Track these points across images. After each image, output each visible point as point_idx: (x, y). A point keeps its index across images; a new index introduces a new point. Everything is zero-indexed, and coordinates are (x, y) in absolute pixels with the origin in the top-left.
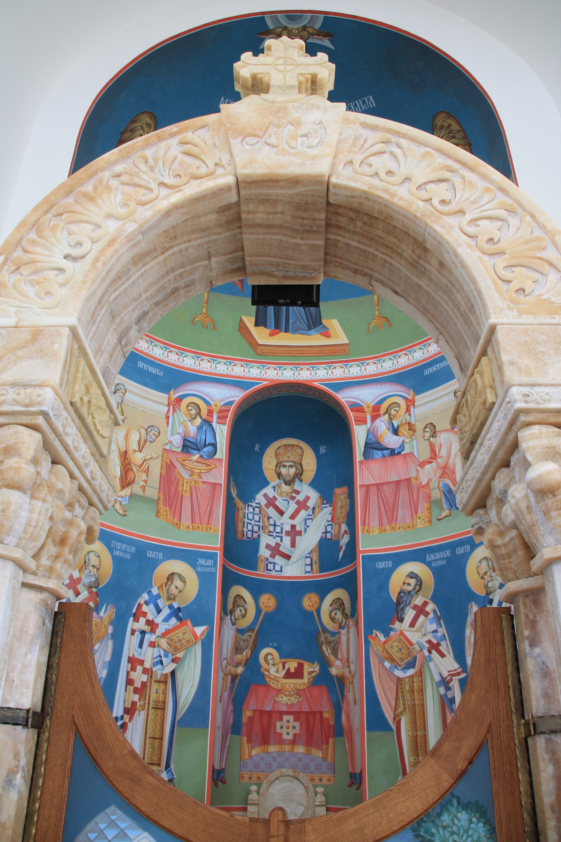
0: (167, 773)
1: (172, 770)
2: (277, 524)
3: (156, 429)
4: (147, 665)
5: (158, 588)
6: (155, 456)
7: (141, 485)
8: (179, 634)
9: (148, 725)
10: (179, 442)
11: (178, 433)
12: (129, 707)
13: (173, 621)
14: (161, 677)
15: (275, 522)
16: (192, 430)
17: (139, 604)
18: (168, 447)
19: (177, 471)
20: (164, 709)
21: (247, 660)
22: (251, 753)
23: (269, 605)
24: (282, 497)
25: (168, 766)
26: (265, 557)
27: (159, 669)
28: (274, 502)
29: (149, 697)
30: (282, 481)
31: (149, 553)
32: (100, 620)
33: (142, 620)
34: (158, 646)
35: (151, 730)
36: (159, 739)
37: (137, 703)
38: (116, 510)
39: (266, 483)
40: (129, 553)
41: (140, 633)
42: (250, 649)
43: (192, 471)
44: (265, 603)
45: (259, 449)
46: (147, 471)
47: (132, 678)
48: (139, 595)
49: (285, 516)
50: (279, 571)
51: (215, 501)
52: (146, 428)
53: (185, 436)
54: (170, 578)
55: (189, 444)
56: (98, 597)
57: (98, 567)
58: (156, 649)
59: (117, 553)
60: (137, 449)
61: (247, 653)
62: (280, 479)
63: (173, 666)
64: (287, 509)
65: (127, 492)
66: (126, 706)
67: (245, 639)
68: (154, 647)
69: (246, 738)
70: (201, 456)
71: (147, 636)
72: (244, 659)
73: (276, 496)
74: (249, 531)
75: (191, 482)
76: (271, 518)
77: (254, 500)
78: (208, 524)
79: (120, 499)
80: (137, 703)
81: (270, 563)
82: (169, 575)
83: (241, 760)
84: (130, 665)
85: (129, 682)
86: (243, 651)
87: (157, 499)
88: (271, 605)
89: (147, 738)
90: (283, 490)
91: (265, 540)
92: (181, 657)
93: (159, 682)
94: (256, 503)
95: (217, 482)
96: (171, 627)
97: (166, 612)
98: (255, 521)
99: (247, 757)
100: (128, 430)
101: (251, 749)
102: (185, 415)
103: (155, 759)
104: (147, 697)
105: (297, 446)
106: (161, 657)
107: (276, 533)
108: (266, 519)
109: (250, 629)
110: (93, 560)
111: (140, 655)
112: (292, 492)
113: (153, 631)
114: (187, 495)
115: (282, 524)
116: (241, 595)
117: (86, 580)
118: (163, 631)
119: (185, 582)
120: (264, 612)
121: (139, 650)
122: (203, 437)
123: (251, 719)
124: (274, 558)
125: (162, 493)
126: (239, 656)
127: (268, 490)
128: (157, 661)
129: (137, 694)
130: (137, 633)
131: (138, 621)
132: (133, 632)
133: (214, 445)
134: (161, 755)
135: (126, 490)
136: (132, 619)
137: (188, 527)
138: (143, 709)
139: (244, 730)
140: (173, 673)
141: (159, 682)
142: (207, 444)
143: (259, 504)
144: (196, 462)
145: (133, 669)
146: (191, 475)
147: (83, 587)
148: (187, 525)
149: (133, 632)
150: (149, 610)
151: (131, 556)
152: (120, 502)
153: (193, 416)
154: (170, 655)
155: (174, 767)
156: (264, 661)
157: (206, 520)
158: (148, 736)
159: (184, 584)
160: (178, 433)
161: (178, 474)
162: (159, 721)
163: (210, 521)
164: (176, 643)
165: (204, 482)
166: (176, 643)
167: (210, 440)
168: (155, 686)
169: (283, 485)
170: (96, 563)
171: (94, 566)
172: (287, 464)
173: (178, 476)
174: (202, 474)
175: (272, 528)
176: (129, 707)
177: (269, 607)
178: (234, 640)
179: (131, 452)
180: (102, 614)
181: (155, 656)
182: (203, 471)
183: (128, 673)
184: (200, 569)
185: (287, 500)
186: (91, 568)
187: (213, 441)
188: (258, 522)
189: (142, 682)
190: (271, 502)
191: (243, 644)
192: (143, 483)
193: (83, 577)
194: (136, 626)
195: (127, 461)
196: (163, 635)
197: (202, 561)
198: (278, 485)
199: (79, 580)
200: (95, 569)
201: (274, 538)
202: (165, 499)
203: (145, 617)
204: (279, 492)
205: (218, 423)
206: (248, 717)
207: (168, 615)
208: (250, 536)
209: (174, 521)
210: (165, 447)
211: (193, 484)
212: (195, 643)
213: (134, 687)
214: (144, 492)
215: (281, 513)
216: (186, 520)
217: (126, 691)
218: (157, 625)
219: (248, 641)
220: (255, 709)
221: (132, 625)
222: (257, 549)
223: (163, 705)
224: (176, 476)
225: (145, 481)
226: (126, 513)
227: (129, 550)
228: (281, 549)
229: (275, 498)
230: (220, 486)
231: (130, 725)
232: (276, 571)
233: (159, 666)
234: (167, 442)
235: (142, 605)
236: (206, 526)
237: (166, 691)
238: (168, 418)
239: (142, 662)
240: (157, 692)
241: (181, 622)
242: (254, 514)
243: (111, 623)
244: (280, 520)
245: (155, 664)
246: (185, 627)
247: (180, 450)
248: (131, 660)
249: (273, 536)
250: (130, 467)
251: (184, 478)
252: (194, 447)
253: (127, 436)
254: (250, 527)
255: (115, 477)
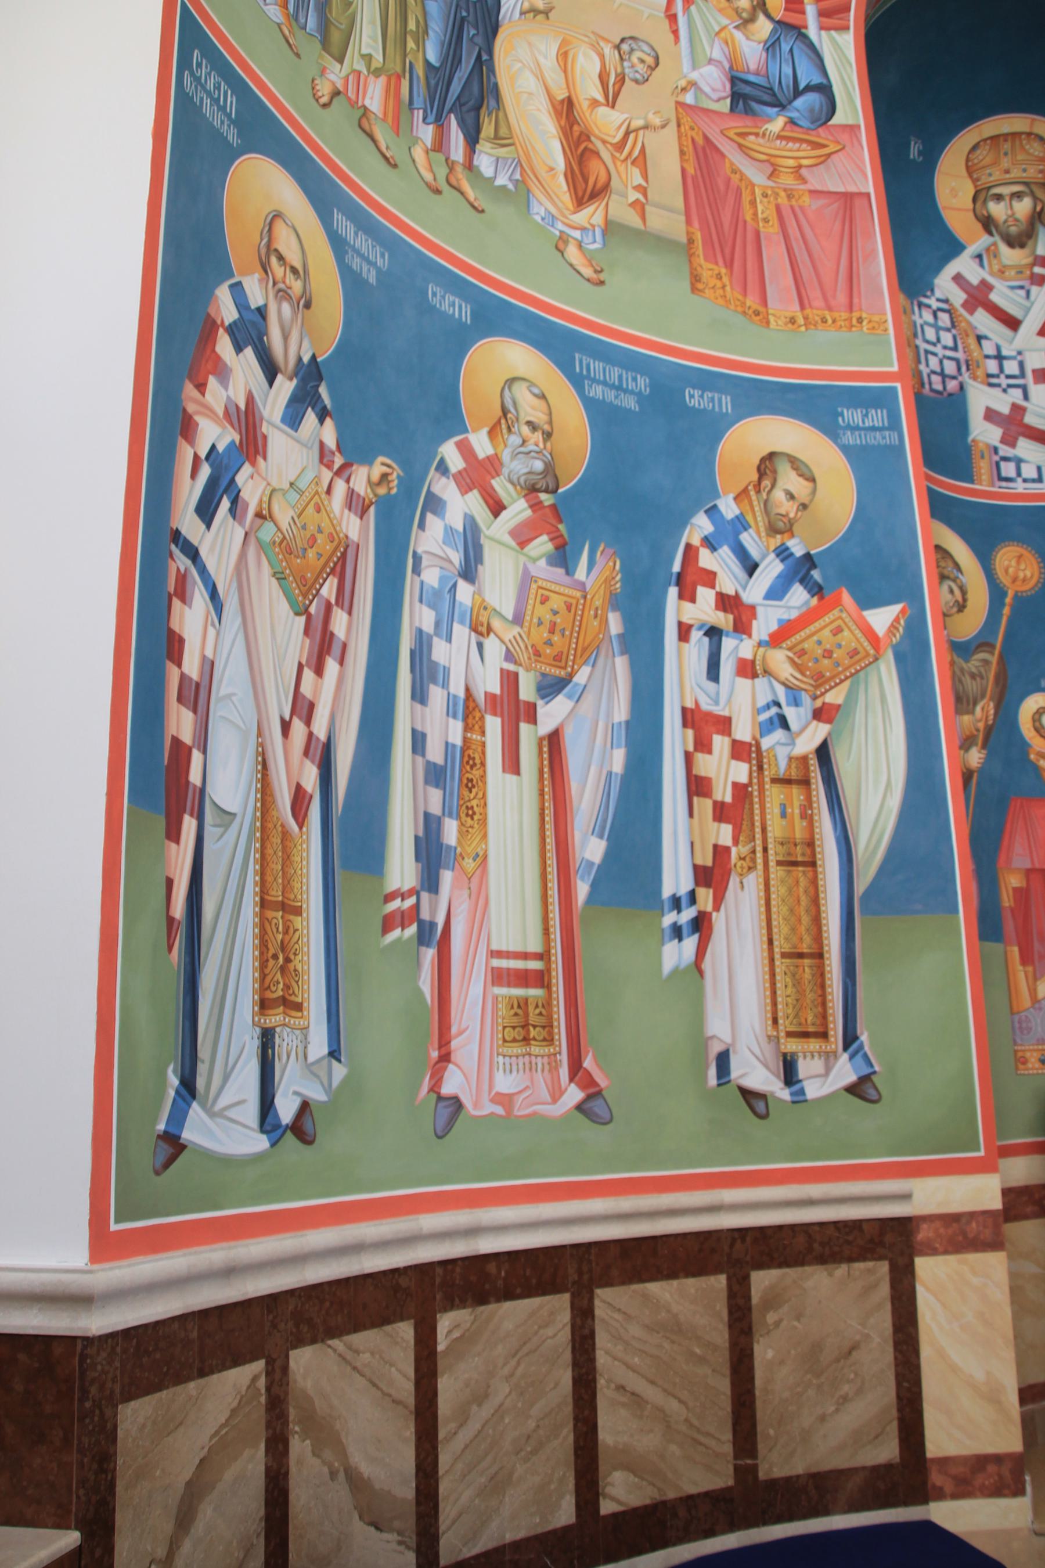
0: (851, 1058)
1: (866, 1048)
2: (1005, 352)
3: (646, 48)
4: (743, 731)
5: (735, 499)
6: (657, 121)
7: (631, 199)
8: (819, 636)
9: (774, 916)
10: (719, 86)
11: (711, 61)
12: (709, 862)
13: (798, 597)
14: (789, 766)
15: (998, 348)
16: (751, 49)
17: (688, 547)
18: (689, 98)
19: (727, 165)
20: (813, 864)
21: (989, 731)
22: (1035, 990)
23: (1021, 575)
24: (1006, 280)
25: (850, 1039)
26: (988, 445)
27: (778, 743)
28: (987, 295)
29: (764, 830)
30: (997, 238)
31: (692, 396)
32: (579, 594)
33: (705, 596)
34: (766, 672)
35: (785, 930)
36: (811, 956)
37: (727, 850)
38: (571, 265)
39: (955, 248)
40: (632, 392)
41: (706, 634)
42: (991, 699)
43: (772, 164)
44: (1011, 570)
45: (920, 153)
46: (641, 161)
47: (703, 774)
48: (683, 520)
49: (1023, 329)
50: (1033, 481)
51: (859, 242)
52: (617, 41)
53: (731, 68)
54: (768, 465)
55: (747, 90)
56: (561, 521)
57: (546, 427)
58: (761, 682)
59: (597, 392)
60: (600, 98)
61: (984, 710)
62: (991, 234)
63: (819, 732)
64: (1028, 310)
65: (592, 215)
66: (699, 862)
67: (974, 670)
68: (754, 676)
69: (1016, 949)
70: (792, 122)
71: (728, 644)
72: (981, 725)
73: (991, 280)
74: (934, 372)
75: (777, 194)
76: (986, 338)
77: (932, 291)
78: (851, 308)
79: (577, 234)
80: (727, 850)
81: (1005, 459)
82: (763, 460)
83: (1012, 1014)
84: (690, 733)
85: (698, 786)
86: (975, 704)
87: (684, 240)
88: (1028, 573)
89: (777, 956)
90: (1006, 262)
91: (981, 399)
92: (839, 701)
93: (787, 781)
94: (938, 300)
95: (852, 189)
96: (794, 614)
97: (771, 569)
98: (945, 348)
99: (1027, 1002)
100: (564, 42)
101: (1035, 979)
102: (720, 11)
103: (810, 1019)
104: (758, 830)
105: (1029, 134)
106: (778, 704)
107: (1008, 377)
108: (972, 341)
109: (982, 643)
110: (529, 408)
111: (716, 703)
112: (1034, 264)
113: (742, 628)
114: (771, 230)
115: (1020, 353)
116: (945, 546)
117: (516, 467)
118: (774, 627)
119: (813, 480)
120: (1010, 594)
121: (711, 686)
122: (788, 70)
123: (1022, 895)
124: (1013, 445)
125: (696, 224)
126: (966, 718)
127: (963, 265)
128: (771, 719)
129: (728, 822)
130: (696, 635)
131: (693, 600)
132: (684, 632)
133: (825, 89)
134: (824, 1004)
135: (590, 210)
136: (673, 591)
137: (792, 321)
138: (750, 869)
139: (1009, 926)
140: (823, 752)
141: (787, 781)
142: (802, 86)
143: (946, 301)
144: (780, 137)
145: (703, 745)
146: (770, 177)
147: (510, 487)
148: (789, 314)
149: (684, 632)
150: (719, 562)
151: (638, 402)
152: (580, 245)
153: (745, 15)
154: (806, 698)
155: (870, 1036)
156: (1033, 733)
157: (841, 297)
158: (777, 950)
159: (810, 485)
160: (711, 61)
161: (735, 171)
162: (804, 900)
163: (856, 300)
164: (817, 661)
165: (813, 192)
166: (817, 661)
167: (807, 75)
168: (775, 795)
169: (1003, 248)
170: (539, 417)
171: (533, 426)
172: (1006, 190)
173: (735, 178)
174: (804, 172)
175: (992, 366)
176: (709, 862)
177: (1024, 580)
178: (949, 674)
179: (585, 105)
180: (581, 573)
181: (761, 703)
182: (805, 162)
183: (688, 758)
184: (850, 439)
185: (1022, 287)
186: (526, 430)
187: (817, 79)
188: (951, 349)
189: (735, 785)
190: (978, 297)
191: (971, 686)
192: (634, 196)
193: (506, 456)
194: (691, 613)
195: (576, 128)
196: (776, 639)
197: (852, 416)
198: (988, 250)
199: (493, 465)
200: (538, 436)
201: (1005, 391)
202: (708, 242)
203: (713, 587)
204: (996, 268)
205: (822, 28)
206: (1015, 889)
207: (779, 577)
208: (939, 387)
209: (748, 303)
210: (681, 99)
211: (782, 200)
212: (876, 659)
213: (715, 803)
214: (643, 218)
215: (1013, 323)
216: (781, 300)
217: (691, 814)
218: (752, 608)
219: (982, 677)
220: (1029, 866)
221: (679, 610)
222: (962, 423)
223: (808, 851)
224: (728, 181)
225: (643, 190)
226: (602, 276)
227: (631, 386)
228: (1029, 419)
229: (986, 286)
230: (866, 202)
231: (719, 920)
232: (1025, 481)
233: (779, 734)
234: (683, 83)
235: (697, 549)
236: (844, 315)
237: (811, 808)
238: (672, 18)
239: (724, 724)
240: (783, 815)
241: (821, 598)
242: (938, 329)
243: (614, 602)
244: (1011, 342)
245: (766, 728)
246: (836, 612)
247: (725, 106)
248: (690, 717)
249: (998, 385)
250: (590, 146)
251: (753, 185)
252: (766, 98)
253: (564, 57)
254: (934, 362)
255: (552, 169)
